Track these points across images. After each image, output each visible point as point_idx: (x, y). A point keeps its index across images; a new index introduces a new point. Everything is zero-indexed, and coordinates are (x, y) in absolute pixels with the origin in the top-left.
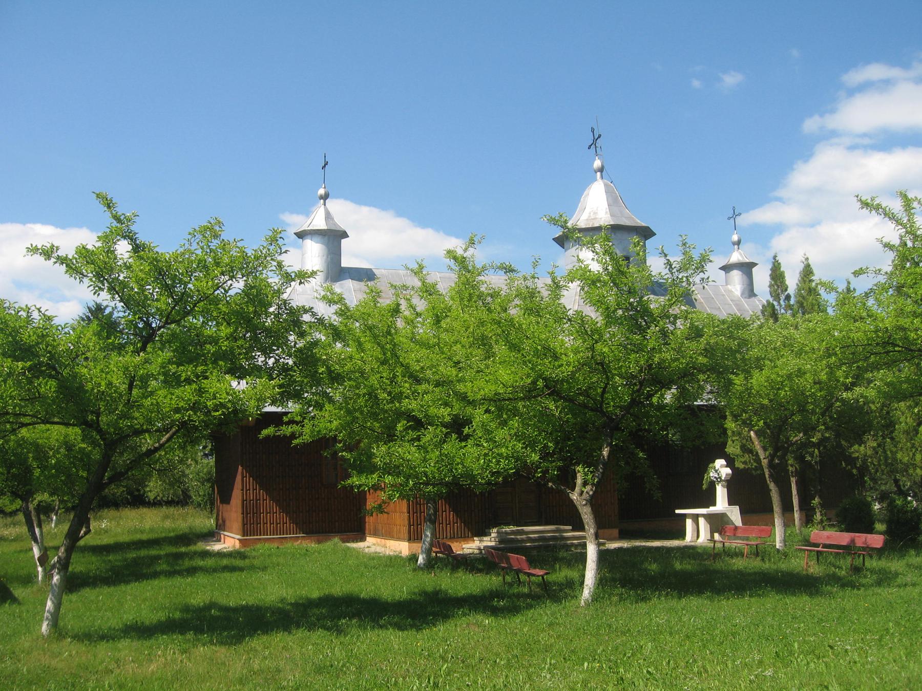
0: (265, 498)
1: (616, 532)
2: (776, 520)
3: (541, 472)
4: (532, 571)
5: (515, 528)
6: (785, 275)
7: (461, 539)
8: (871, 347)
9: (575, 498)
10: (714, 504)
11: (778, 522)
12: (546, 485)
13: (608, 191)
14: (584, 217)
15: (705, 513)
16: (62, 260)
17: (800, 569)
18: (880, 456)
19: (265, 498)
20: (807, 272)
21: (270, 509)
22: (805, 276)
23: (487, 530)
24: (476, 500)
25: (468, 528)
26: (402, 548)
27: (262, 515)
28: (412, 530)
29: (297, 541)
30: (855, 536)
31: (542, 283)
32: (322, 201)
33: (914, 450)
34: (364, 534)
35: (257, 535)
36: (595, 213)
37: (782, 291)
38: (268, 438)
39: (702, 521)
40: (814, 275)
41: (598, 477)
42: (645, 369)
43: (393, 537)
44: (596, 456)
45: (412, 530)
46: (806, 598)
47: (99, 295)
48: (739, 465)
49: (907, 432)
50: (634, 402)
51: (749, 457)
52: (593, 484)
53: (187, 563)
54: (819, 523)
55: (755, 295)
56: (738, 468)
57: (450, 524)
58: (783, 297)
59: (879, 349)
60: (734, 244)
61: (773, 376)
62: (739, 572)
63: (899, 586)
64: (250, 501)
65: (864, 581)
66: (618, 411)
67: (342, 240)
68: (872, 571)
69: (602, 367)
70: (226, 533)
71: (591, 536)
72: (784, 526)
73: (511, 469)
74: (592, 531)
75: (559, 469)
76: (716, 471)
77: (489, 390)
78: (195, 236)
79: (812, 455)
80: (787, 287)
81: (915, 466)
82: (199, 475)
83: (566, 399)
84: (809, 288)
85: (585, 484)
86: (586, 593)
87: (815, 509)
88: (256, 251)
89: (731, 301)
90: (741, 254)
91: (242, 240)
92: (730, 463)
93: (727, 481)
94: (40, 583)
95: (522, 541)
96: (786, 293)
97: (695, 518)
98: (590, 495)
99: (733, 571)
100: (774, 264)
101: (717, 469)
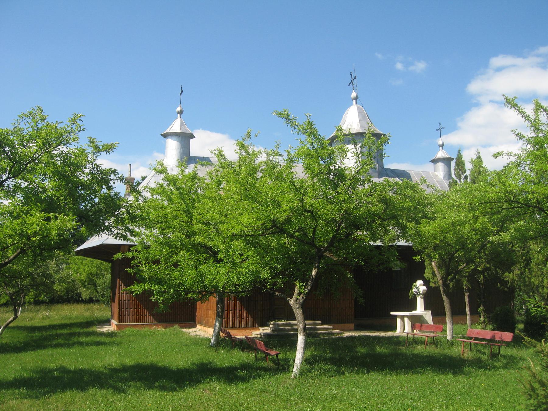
0: (133, 299)
1: (352, 326)
2: (447, 321)
5: (284, 322)
7: (251, 328)
9: (292, 303)
10: (415, 309)
12: (274, 293)
13: (360, 112)
15: (408, 315)
19: (133, 299)
23: (267, 323)
27: (131, 309)
29: (153, 327)
30: (495, 333)
31: (281, 161)
32: (179, 115)
33: (542, 276)
36: (351, 125)
37: (462, 173)
38: (118, 259)
39: (406, 319)
43: (209, 326)
46: (450, 376)
48: (432, 285)
57: (244, 318)
58: (463, 177)
60: (440, 146)
64: (124, 301)
67: (191, 140)
76: (417, 288)
78: (23, 118)
81: (543, 287)
82: (104, 284)
85: (300, 294)
89: (437, 181)
90: (444, 153)
91: (62, 122)
93: (424, 294)
95: (289, 330)
96: (465, 175)
101: (417, 286)
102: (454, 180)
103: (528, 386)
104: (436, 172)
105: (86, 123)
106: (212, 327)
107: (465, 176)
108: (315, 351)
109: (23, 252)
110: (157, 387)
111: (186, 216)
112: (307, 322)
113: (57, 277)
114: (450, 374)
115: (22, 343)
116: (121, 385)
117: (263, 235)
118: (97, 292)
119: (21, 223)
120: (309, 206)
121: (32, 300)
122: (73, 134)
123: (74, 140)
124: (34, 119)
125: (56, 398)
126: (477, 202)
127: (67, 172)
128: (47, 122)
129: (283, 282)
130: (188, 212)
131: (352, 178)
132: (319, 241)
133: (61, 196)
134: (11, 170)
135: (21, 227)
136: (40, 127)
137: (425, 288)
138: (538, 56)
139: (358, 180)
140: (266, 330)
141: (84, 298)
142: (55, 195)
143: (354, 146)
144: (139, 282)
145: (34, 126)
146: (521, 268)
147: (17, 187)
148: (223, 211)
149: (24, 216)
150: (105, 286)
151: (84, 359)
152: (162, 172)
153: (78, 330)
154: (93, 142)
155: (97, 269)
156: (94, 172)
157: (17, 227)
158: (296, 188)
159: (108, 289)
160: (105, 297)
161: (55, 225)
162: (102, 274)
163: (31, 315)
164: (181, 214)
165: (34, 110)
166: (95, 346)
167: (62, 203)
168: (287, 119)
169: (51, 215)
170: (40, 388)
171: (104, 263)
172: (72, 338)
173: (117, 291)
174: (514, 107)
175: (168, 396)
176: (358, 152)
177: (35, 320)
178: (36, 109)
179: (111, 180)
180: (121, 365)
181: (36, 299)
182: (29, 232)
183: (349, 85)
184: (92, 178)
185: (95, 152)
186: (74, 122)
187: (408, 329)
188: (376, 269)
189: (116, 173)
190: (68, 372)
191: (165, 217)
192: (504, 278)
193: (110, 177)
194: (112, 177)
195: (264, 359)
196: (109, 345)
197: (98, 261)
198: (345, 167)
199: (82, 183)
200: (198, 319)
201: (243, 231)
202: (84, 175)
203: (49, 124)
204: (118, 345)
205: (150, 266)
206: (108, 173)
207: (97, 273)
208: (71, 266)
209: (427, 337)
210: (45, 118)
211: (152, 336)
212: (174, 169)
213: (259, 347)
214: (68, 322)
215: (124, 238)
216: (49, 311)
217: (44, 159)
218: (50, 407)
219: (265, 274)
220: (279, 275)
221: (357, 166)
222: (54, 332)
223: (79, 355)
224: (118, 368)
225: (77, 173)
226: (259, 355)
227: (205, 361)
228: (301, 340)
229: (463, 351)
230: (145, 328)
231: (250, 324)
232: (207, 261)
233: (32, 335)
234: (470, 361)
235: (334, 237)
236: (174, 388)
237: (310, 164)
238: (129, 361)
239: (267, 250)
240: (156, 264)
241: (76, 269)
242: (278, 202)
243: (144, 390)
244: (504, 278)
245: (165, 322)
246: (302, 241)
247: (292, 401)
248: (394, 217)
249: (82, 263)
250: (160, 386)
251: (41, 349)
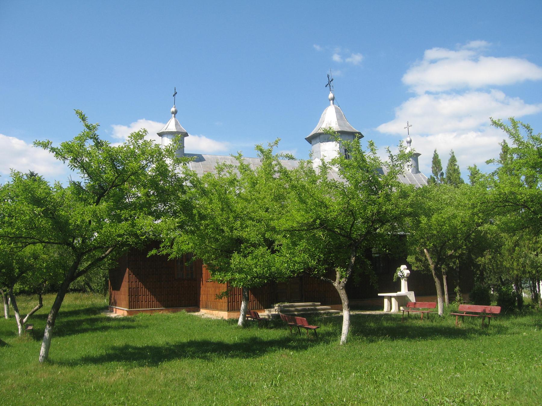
0: (142, 287)
3: (317, 271)
4: (309, 327)
6: (441, 161)
8: (497, 203)
10: (400, 290)
11: (439, 300)
13: (337, 112)
16: (53, 150)
17: (454, 326)
18: (493, 263)
19: (142, 287)
20: (453, 160)
21: (145, 294)
23: (272, 305)
24: (266, 287)
25: (261, 304)
26: (224, 315)
27: (140, 296)
28: (230, 305)
29: (160, 311)
32: (173, 115)
34: (200, 307)
35: (137, 308)
37: (439, 171)
39: (393, 300)
40: (457, 162)
41: (349, 274)
42: (375, 214)
45: (230, 305)
46: (462, 340)
47: (74, 170)
49: (509, 250)
50: (368, 232)
51: (420, 264)
52: (346, 278)
53: (100, 324)
54: (459, 301)
55: (419, 172)
56: (414, 270)
58: (439, 174)
59: (501, 204)
61: (439, 218)
62: (420, 327)
63: (511, 334)
65: (490, 332)
66: (359, 237)
67: (185, 138)
68: (494, 327)
69: (352, 213)
70: (116, 307)
71: (345, 307)
72: (443, 302)
74: (346, 303)
75: (326, 269)
76: (401, 272)
77: (288, 225)
79: (454, 263)
80: (442, 168)
83: (329, 230)
84: (454, 169)
85: (341, 277)
86: (343, 337)
87: (456, 293)
92: (409, 267)
93: (407, 277)
94: (20, 335)
96: (441, 172)
97: (390, 298)
98: (345, 284)
99: (416, 327)
100: (434, 155)
101: (401, 270)
102: (432, 177)
107: (441, 173)
137: (408, 272)
138: (470, 49)
244: (478, 262)
245: (171, 307)
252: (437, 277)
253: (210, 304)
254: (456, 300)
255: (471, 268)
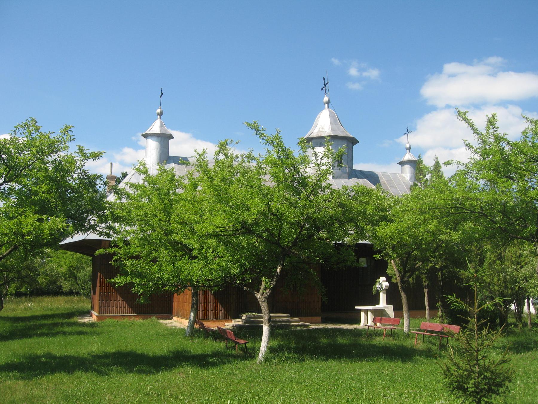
0: (113, 291)
2: (404, 315)
9: (258, 297)
10: (378, 304)
14: (316, 130)
19: (113, 291)
22: (436, 168)
23: (240, 315)
27: (111, 301)
29: (131, 318)
35: (108, 314)
36: (322, 128)
43: (185, 318)
44: (273, 272)
46: (399, 363)
52: (270, 289)
56: (393, 282)
60: (407, 149)
64: (104, 293)
67: (170, 140)
73: (219, 278)
76: (380, 284)
78: (19, 129)
85: (265, 289)
86: (261, 356)
87: (438, 309)
88: (54, 138)
90: (411, 155)
91: (54, 132)
92: (389, 279)
98: (268, 295)
101: (380, 282)
103: (445, 368)
104: (404, 173)
105: (75, 133)
106: (187, 318)
108: (282, 341)
109: (16, 248)
110: (136, 371)
111: (165, 215)
112: (271, 315)
113: (41, 270)
114: (399, 361)
115: (8, 333)
116: (104, 369)
117: (235, 235)
118: (78, 285)
119: (17, 223)
120: (275, 210)
121: (14, 292)
122: (64, 143)
123: (64, 149)
124: (29, 129)
125: (47, 379)
126: (427, 208)
127: (58, 177)
128: (41, 132)
129: (251, 278)
130: (167, 213)
131: (313, 185)
132: (284, 241)
133: (52, 198)
134: (7, 175)
135: (17, 227)
136: (34, 137)
137: (387, 284)
138: (488, 65)
139: (320, 187)
140: (238, 322)
141: (64, 290)
142: (46, 198)
143: (315, 157)
144: (122, 275)
145: (29, 136)
146: (476, 266)
147: (12, 190)
148: (198, 212)
149: (19, 217)
150: (85, 279)
151: (68, 347)
152: (144, 173)
153: (60, 321)
154: (81, 150)
155: (77, 262)
156: (81, 177)
157: (13, 227)
158: (263, 194)
159: (88, 282)
160: (85, 289)
161: (47, 226)
162: (83, 267)
163: (13, 306)
164: (160, 213)
165: (28, 121)
166: (77, 335)
167: (53, 205)
168: (257, 130)
169: (44, 217)
170: (31, 371)
171: (85, 256)
172: (55, 328)
173: (98, 284)
174: (465, 121)
175: (147, 378)
176: (319, 163)
177: (17, 311)
178: (30, 120)
179: (97, 184)
180: (103, 352)
181: (18, 291)
182: (24, 231)
183: (322, 90)
184: (80, 183)
185: (83, 159)
186: (65, 132)
187: (370, 323)
188: (335, 267)
189: (102, 179)
190: (55, 358)
191: (146, 214)
192: (460, 275)
193: (96, 182)
194: (98, 181)
195: (233, 348)
196: (91, 334)
197: (79, 255)
198: (307, 175)
199: (71, 187)
200: (174, 310)
201: (216, 231)
202: (73, 180)
203: (42, 134)
204: (98, 334)
205: (133, 261)
206: (94, 178)
207: (77, 265)
208: (53, 259)
209: (385, 329)
210: (39, 129)
211: (131, 326)
212: (153, 168)
213: (229, 336)
214: (49, 313)
215: (108, 235)
216: (31, 303)
217: (37, 165)
218: (42, 386)
219: (234, 271)
220: (248, 271)
221: (318, 175)
222: (38, 322)
223: (64, 343)
224: (101, 354)
225: (67, 178)
226: (229, 345)
227: (180, 349)
228: (266, 330)
229: (416, 342)
230: (124, 319)
231: (223, 316)
232: (183, 257)
233: (16, 324)
234: (420, 351)
235: (297, 238)
236: (151, 372)
237: (276, 173)
238: (111, 349)
239: (238, 248)
240: (138, 260)
241: (57, 261)
242: (247, 206)
243: (125, 373)
244: (460, 275)
246: (269, 241)
247: (256, 383)
248: (351, 220)
249: (63, 256)
250: (139, 370)
251: (27, 337)
252: (403, 291)
253: (179, 312)
254: (438, 316)
255: (455, 282)
